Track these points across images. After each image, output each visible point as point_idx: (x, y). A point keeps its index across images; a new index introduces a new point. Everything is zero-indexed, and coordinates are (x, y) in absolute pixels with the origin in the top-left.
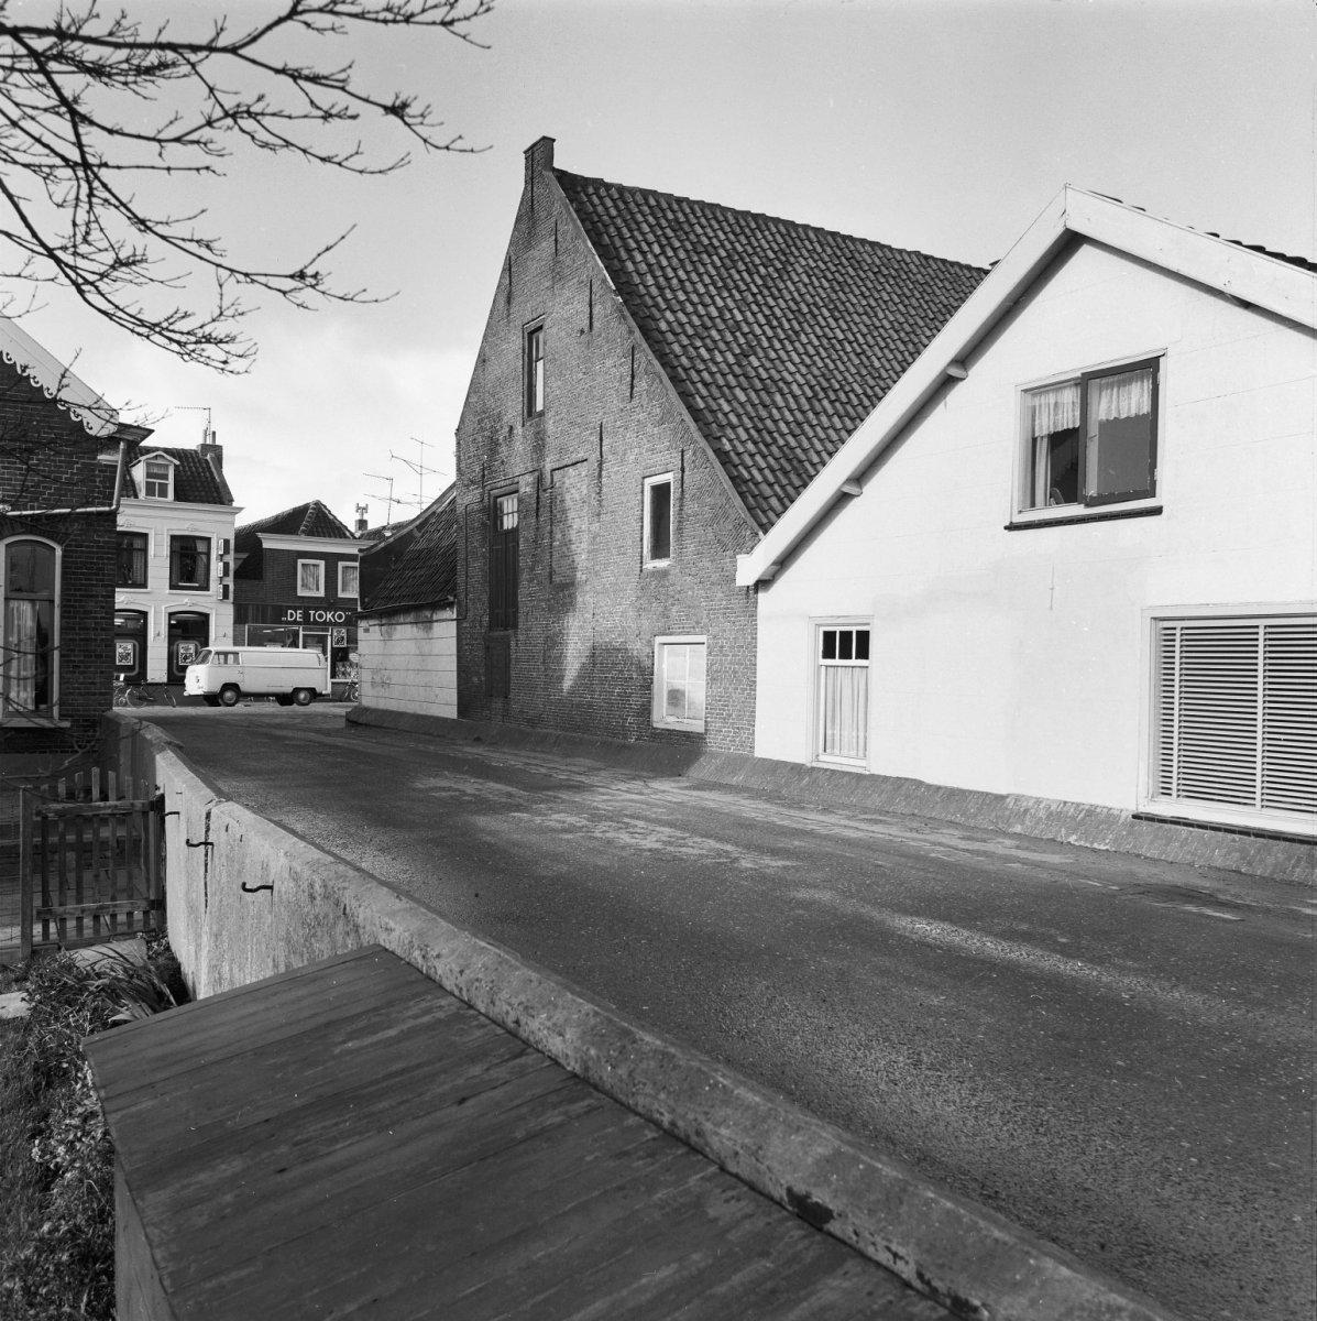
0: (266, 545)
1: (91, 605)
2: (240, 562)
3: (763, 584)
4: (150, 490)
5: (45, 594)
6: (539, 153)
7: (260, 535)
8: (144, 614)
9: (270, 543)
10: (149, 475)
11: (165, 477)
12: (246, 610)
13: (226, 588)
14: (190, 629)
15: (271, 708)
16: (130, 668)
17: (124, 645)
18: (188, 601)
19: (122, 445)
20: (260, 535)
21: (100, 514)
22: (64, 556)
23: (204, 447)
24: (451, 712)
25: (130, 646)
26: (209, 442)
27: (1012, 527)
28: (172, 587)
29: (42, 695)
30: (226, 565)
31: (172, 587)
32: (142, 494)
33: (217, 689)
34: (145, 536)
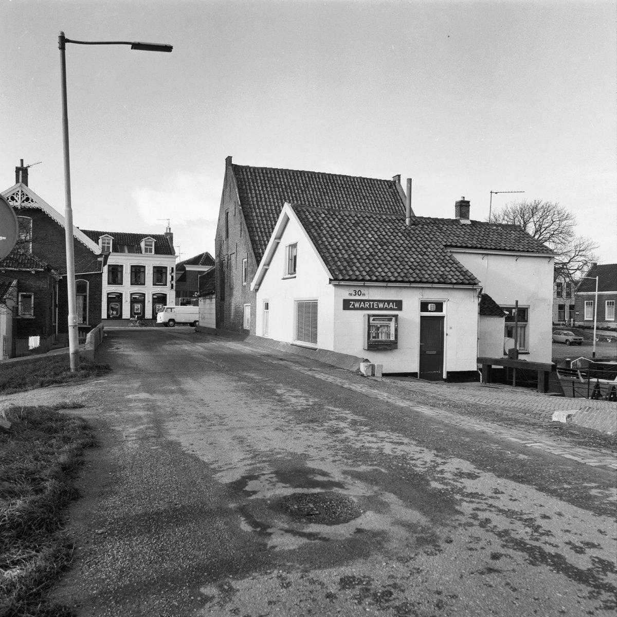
0: (187, 269)
1: (96, 296)
2: (180, 275)
3: (257, 290)
4: (146, 250)
5: (85, 294)
6: (229, 159)
7: (185, 266)
8: (144, 294)
9: (189, 268)
10: (146, 245)
11: (151, 246)
12: (180, 292)
13: (172, 285)
14: (161, 299)
15: (189, 327)
16: (140, 314)
17: (137, 305)
18: (159, 290)
19: (103, 256)
20: (185, 266)
21: (98, 273)
22: (89, 284)
23: (167, 234)
24: (214, 326)
25: (139, 306)
26: (168, 232)
27: (284, 279)
28: (154, 285)
29: (84, 319)
30: (172, 277)
31: (154, 285)
32: (143, 252)
33: (167, 320)
34: (144, 267)
